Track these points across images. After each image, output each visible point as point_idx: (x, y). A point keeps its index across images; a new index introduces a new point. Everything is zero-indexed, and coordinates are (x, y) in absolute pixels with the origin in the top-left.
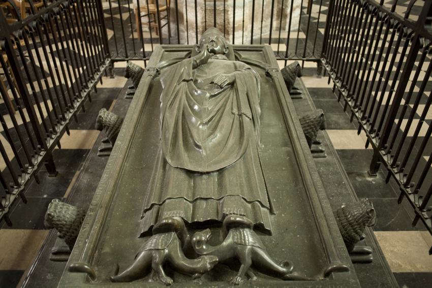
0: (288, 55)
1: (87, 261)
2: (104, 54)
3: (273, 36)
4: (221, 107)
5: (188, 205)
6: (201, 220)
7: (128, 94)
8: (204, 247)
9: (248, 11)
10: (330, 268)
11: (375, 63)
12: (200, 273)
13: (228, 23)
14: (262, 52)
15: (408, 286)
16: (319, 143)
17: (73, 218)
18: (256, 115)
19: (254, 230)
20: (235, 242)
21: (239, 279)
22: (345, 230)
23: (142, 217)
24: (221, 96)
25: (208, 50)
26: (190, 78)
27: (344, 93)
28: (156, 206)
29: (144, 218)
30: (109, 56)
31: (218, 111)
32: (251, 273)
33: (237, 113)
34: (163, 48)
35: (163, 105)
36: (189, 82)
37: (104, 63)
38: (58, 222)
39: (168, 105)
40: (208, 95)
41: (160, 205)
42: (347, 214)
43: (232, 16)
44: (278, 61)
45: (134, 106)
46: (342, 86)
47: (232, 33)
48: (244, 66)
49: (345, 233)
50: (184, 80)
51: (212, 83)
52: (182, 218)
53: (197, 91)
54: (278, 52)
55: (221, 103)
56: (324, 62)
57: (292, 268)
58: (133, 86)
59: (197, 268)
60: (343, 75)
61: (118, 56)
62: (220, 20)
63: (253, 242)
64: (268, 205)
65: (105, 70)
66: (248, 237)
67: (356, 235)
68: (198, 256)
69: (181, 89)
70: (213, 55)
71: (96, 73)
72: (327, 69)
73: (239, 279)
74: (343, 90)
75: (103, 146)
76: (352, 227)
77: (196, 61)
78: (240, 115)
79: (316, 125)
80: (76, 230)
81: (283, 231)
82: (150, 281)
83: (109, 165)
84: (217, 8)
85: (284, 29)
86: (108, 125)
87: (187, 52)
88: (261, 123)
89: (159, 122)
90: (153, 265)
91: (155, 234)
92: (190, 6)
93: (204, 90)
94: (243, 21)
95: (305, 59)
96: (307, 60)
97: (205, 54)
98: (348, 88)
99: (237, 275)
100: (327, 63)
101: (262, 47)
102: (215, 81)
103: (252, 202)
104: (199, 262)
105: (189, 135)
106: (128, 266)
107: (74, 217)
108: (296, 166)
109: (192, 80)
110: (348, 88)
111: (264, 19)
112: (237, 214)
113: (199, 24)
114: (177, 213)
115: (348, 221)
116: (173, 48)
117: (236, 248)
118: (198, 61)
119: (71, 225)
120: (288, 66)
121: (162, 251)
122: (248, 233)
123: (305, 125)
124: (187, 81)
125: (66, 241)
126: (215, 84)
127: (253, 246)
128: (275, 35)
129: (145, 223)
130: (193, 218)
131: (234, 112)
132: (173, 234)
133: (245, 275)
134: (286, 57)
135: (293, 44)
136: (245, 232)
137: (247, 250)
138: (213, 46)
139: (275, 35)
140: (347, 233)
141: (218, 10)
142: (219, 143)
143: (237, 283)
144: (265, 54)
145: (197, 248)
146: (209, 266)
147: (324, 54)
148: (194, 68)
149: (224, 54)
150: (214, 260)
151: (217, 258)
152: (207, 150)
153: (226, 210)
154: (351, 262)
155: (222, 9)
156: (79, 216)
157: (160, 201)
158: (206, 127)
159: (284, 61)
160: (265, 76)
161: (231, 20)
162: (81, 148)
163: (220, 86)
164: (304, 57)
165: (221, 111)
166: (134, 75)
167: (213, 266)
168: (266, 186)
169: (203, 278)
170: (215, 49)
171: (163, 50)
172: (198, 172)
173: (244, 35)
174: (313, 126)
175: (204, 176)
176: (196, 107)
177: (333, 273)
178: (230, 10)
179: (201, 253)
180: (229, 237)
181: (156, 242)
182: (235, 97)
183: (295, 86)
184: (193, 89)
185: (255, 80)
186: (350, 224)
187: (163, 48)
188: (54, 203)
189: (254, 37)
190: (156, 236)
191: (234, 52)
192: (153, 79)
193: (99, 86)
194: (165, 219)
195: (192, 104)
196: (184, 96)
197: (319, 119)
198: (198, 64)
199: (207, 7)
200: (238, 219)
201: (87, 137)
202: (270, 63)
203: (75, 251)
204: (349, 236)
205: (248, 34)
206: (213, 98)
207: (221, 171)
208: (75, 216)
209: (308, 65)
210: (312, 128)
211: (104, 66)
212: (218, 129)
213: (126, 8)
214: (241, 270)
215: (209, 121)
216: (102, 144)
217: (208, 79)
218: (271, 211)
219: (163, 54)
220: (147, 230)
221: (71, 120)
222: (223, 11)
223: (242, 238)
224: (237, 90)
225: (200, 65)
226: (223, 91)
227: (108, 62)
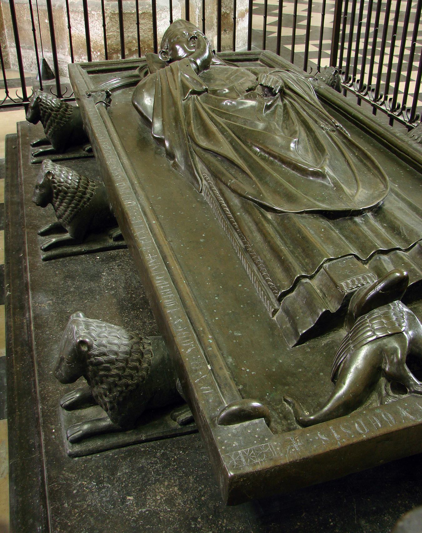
11: (348, 27)
38: (101, 359)
92: (73, 11)
119: (126, 361)
166: (50, 114)
213: (288, 49)
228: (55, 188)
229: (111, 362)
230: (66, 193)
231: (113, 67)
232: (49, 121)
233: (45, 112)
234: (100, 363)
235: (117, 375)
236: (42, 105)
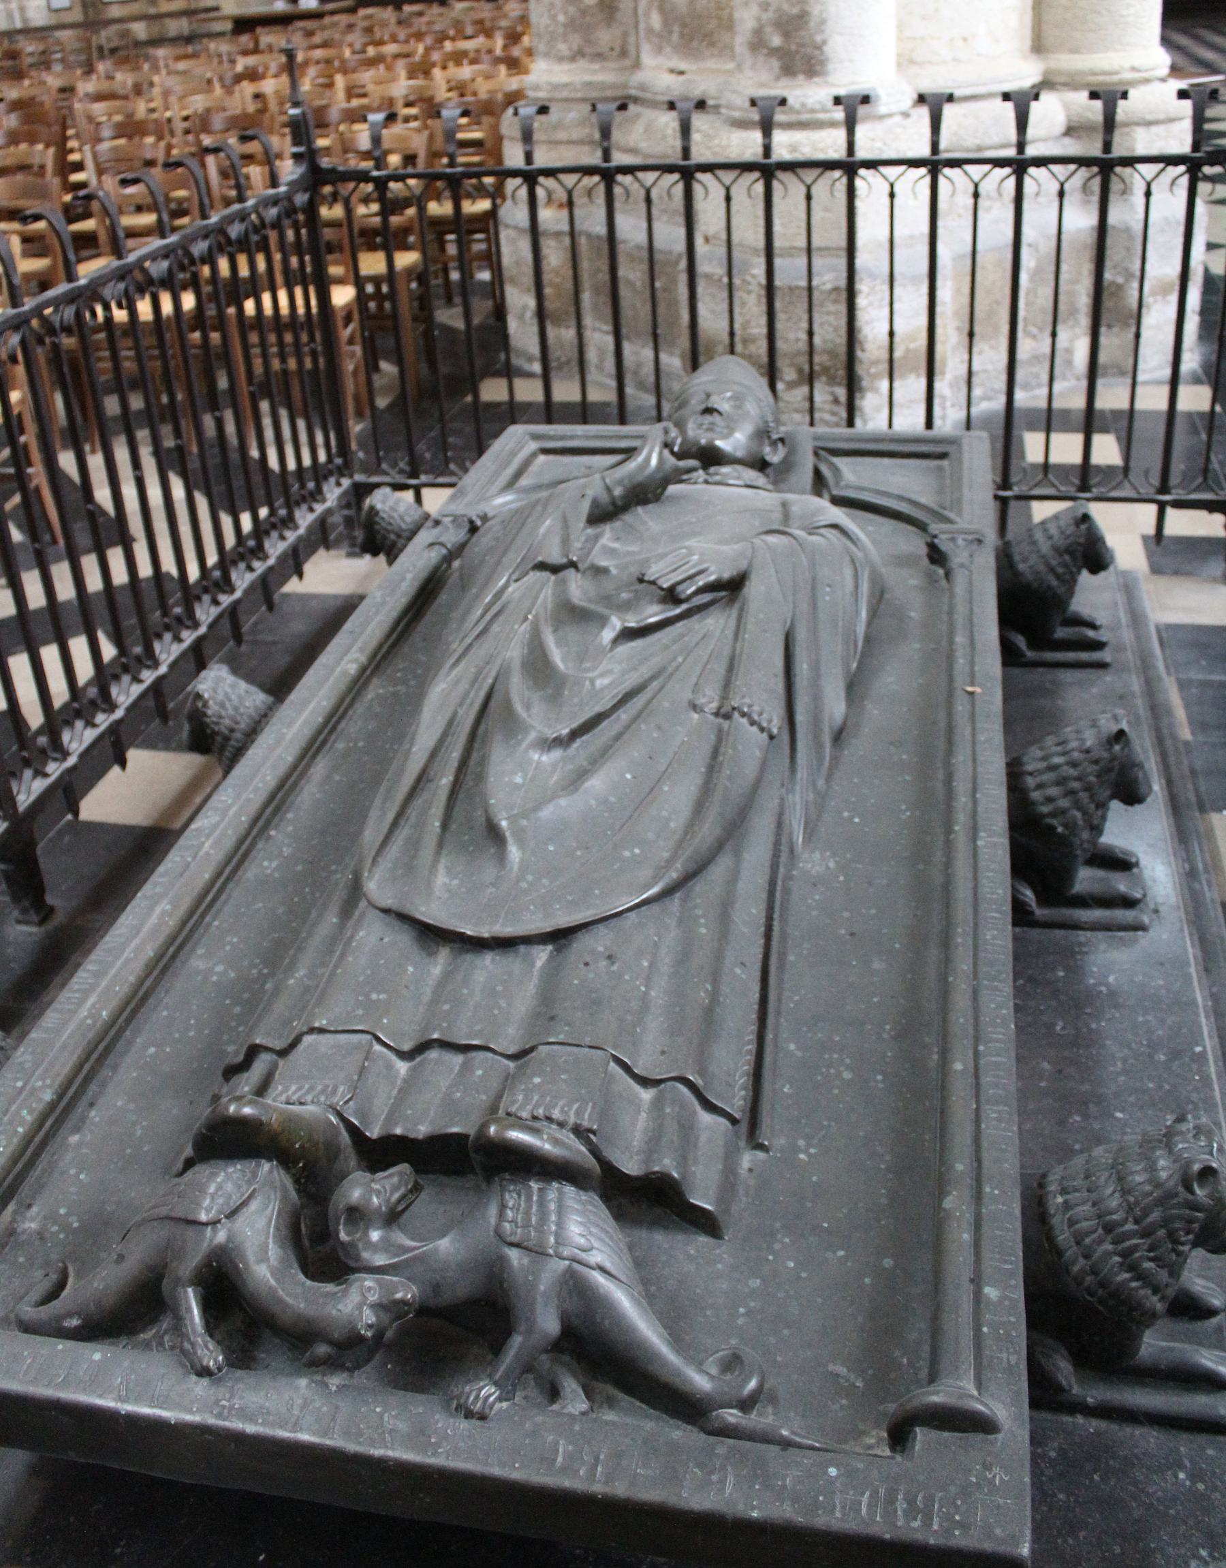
5: (389, 1066)
15: (7, 831)
34: (536, 437)
36: (561, 575)
42: (1103, 1179)
49: (1082, 1270)
51: (641, 581)
54: (1046, 467)
71: (275, 534)
79: (1092, 779)
86: (226, 732)
94: (971, 335)
97: (654, 461)
117: (502, 1260)
118: (618, 492)
124: (555, 569)
139: (1029, 397)
140: (1094, 1272)
145: (343, 1236)
160: (926, 561)
170: (718, 443)
174: (1076, 785)
185: (848, 572)
186: (1109, 1228)
191: (816, 454)
204: (1102, 1285)
227: (338, 491)
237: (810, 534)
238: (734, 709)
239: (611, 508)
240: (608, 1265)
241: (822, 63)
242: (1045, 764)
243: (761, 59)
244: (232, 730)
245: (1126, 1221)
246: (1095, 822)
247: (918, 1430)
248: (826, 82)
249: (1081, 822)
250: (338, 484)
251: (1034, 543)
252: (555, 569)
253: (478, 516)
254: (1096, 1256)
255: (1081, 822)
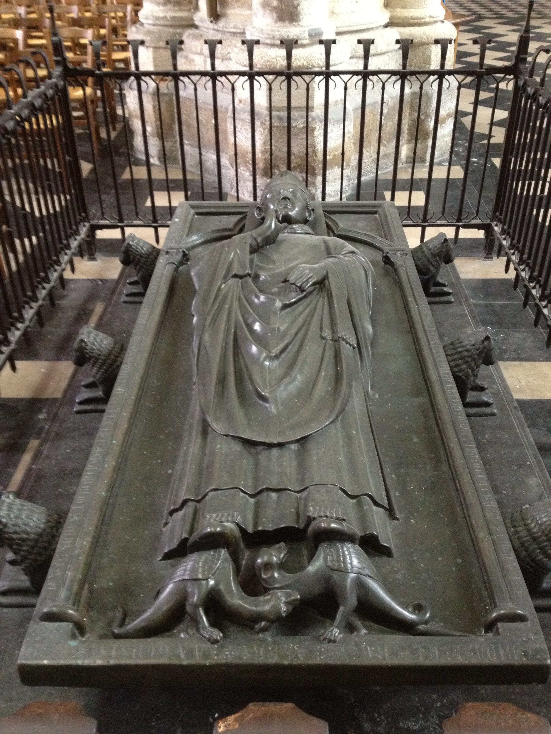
0: (429, 217)
1: (71, 601)
2: (77, 213)
3: (401, 176)
4: (302, 326)
6: (270, 527)
7: (127, 295)
8: (276, 575)
9: (352, 127)
10: (494, 615)
12: (269, 620)
13: (315, 152)
14: (377, 216)
16: (482, 389)
17: (40, 528)
18: (365, 339)
19: (361, 545)
20: (329, 567)
21: (336, 632)
22: (527, 551)
23: (166, 524)
24: (300, 307)
25: (277, 217)
26: (247, 271)
27: (534, 292)
28: (191, 504)
29: (169, 525)
30: (86, 219)
31: (296, 334)
32: (358, 623)
33: (329, 337)
34: (193, 207)
35: (198, 321)
36: (244, 279)
37: (77, 232)
39: (208, 322)
40: (279, 304)
41: (198, 501)
42: (530, 521)
43: (321, 138)
44: (405, 229)
45: (144, 322)
46: (532, 279)
47: (321, 172)
48: (344, 247)
50: (235, 276)
51: (285, 281)
52: (238, 525)
53: (258, 298)
55: (301, 319)
56: (497, 229)
57: (428, 615)
58: (136, 278)
59: (264, 611)
60: (532, 257)
61: (103, 218)
62: (298, 148)
63: (359, 566)
64: (385, 503)
65: (80, 246)
66: (351, 559)
67: (545, 560)
68: (266, 591)
69: (230, 294)
70: (285, 228)
72: (504, 243)
73: (336, 632)
74: (532, 285)
75: (85, 394)
76: (538, 544)
77: (255, 239)
78: (336, 340)
80: (45, 548)
81: (412, 550)
82: (182, 635)
83: (103, 431)
84: (293, 124)
85: (423, 161)
87: (239, 217)
88: (373, 353)
89: (191, 354)
90: (188, 608)
91: (192, 552)
93: (273, 294)
95: (460, 224)
96: (466, 226)
97: (273, 226)
98: (542, 283)
99: (332, 625)
100: (503, 232)
101: (380, 206)
102: (292, 279)
103: (359, 496)
104: (268, 601)
105: (247, 377)
106: (144, 611)
107: (42, 526)
108: (437, 433)
109: (249, 275)
110: (542, 283)
111: (384, 142)
112: (331, 518)
113: (259, 155)
114: (228, 515)
115: (531, 534)
116: (210, 207)
117: (330, 577)
118: (259, 240)
119: (36, 541)
120: (427, 242)
121: (204, 582)
122: (351, 550)
123: (455, 356)
124: (241, 277)
125: (24, 570)
126: (292, 284)
127: (360, 573)
128: (404, 175)
129: (172, 532)
130: (256, 524)
131: (325, 334)
132: (223, 552)
133: (346, 627)
134: (425, 220)
135: (437, 191)
136: (345, 549)
137: (349, 580)
138: (286, 207)
140: (529, 556)
141: (294, 127)
142: (300, 392)
143: (332, 638)
144: (383, 219)
145: (264, 576)
146: (283, 608)
147: (498, 214)
148: (252, 252)
149: (306, 221)
150: (292, 598)
151: (297, 593)
152: (279, 402)
153: (312, 511)
154: (534, 610)
155: (301, 126)
156: (50, 524)
157: (197, 495)
158: (276, 363)
159: (419, 229)
161: (320, 147)
162: (37, 397)
163: (300, 287)
164: (459, 220)
165: (300, 336)
166: (139, 261)
167: (290, 608)
168: (382, 469)
169: (272, 631)
170: (290, 213)
171: (192, 211)
172: (263, 444)
173: (344, 174)
174: (469, 359)
175: (275, 452)
176: (257, 327)
177: (499, 624)
178: (318, 127)
179: (271, 585)
180: (319, 556)
181: (193, 567)
182: (326, 307)
183: (440, 280)
184: (252, 292)
185: (363, 273)
187: (193, 207)
188: (8, 500)
189: (363, 179)
190: (194, 557)
192: (176, 270)
193: (68, 275)
194: (210, 525)
195: (249, 321)
196: (236, 304)
197: (482, 346)
198: (260, 245)
199: (273, 121)
200: (333, 525)
201: (48, 376)
202: (392, 240)
203: (49, 585)
204: (533, 561)
205: (351, 172)
206: (288, 310)
207: (303, 441)
208: (45, 523)
209: (465, 234)
210: (468, 362)
211: (77, 237)
212: (298, 367)
214: (339, 616)
215: (281, 352)
216: (83, 389)
217: (278, 274)
218: (390, 512)
219: (192, 219)
220: (176, 546)
221: (18, 342)
222: (304, 130)
223: (340, 560)
224: (330, 296)
225: (262, 247)
226: (305, 297)
228: (87, 353)
229: (23, 540)
230: (97, 359)
231: (222, 210)
232: (138, 266)
233: (135, 257)
234: (13, 539)
235: (27, 551)
236: (131, 251)
237: (345, 256)
238: (340, 337)
239: (257, 247)
240: (370, 574)
241: (298, 15)
242: (455, 351)
243: (268, 12)
244: (99, 355)
245: (542, 536)
246: (476, 373)
247: (498, 624)
248: (299, 25)
249: (471, 374)
250: (84, 226)
251: (423, 252)
252: (241, 277)
253: (186, 249)
254: (530, 550)
255: (471, 374)
